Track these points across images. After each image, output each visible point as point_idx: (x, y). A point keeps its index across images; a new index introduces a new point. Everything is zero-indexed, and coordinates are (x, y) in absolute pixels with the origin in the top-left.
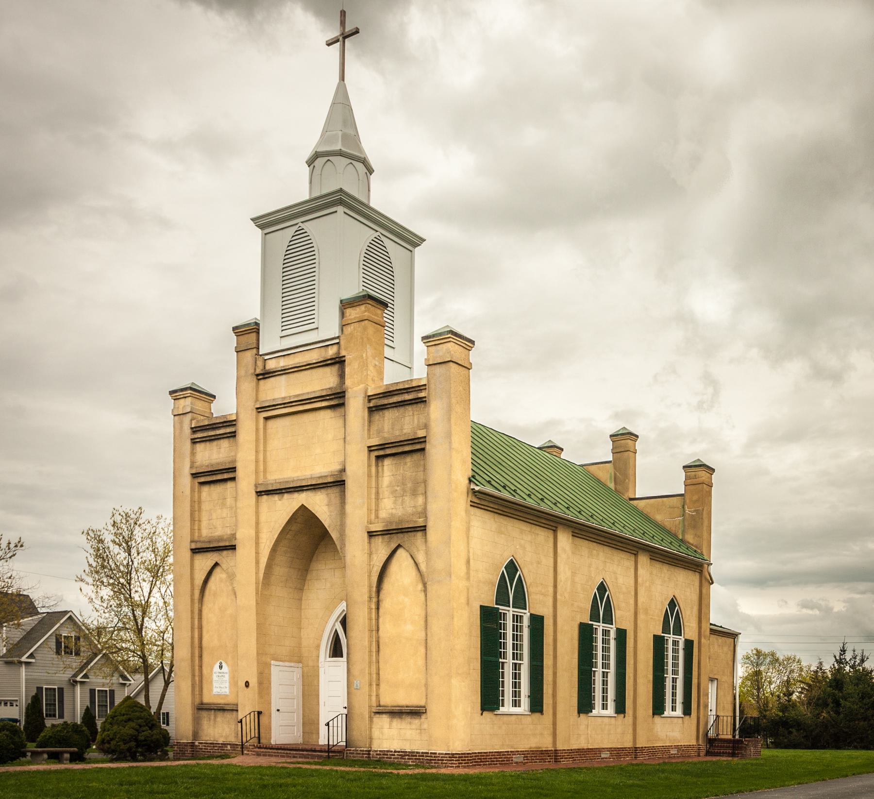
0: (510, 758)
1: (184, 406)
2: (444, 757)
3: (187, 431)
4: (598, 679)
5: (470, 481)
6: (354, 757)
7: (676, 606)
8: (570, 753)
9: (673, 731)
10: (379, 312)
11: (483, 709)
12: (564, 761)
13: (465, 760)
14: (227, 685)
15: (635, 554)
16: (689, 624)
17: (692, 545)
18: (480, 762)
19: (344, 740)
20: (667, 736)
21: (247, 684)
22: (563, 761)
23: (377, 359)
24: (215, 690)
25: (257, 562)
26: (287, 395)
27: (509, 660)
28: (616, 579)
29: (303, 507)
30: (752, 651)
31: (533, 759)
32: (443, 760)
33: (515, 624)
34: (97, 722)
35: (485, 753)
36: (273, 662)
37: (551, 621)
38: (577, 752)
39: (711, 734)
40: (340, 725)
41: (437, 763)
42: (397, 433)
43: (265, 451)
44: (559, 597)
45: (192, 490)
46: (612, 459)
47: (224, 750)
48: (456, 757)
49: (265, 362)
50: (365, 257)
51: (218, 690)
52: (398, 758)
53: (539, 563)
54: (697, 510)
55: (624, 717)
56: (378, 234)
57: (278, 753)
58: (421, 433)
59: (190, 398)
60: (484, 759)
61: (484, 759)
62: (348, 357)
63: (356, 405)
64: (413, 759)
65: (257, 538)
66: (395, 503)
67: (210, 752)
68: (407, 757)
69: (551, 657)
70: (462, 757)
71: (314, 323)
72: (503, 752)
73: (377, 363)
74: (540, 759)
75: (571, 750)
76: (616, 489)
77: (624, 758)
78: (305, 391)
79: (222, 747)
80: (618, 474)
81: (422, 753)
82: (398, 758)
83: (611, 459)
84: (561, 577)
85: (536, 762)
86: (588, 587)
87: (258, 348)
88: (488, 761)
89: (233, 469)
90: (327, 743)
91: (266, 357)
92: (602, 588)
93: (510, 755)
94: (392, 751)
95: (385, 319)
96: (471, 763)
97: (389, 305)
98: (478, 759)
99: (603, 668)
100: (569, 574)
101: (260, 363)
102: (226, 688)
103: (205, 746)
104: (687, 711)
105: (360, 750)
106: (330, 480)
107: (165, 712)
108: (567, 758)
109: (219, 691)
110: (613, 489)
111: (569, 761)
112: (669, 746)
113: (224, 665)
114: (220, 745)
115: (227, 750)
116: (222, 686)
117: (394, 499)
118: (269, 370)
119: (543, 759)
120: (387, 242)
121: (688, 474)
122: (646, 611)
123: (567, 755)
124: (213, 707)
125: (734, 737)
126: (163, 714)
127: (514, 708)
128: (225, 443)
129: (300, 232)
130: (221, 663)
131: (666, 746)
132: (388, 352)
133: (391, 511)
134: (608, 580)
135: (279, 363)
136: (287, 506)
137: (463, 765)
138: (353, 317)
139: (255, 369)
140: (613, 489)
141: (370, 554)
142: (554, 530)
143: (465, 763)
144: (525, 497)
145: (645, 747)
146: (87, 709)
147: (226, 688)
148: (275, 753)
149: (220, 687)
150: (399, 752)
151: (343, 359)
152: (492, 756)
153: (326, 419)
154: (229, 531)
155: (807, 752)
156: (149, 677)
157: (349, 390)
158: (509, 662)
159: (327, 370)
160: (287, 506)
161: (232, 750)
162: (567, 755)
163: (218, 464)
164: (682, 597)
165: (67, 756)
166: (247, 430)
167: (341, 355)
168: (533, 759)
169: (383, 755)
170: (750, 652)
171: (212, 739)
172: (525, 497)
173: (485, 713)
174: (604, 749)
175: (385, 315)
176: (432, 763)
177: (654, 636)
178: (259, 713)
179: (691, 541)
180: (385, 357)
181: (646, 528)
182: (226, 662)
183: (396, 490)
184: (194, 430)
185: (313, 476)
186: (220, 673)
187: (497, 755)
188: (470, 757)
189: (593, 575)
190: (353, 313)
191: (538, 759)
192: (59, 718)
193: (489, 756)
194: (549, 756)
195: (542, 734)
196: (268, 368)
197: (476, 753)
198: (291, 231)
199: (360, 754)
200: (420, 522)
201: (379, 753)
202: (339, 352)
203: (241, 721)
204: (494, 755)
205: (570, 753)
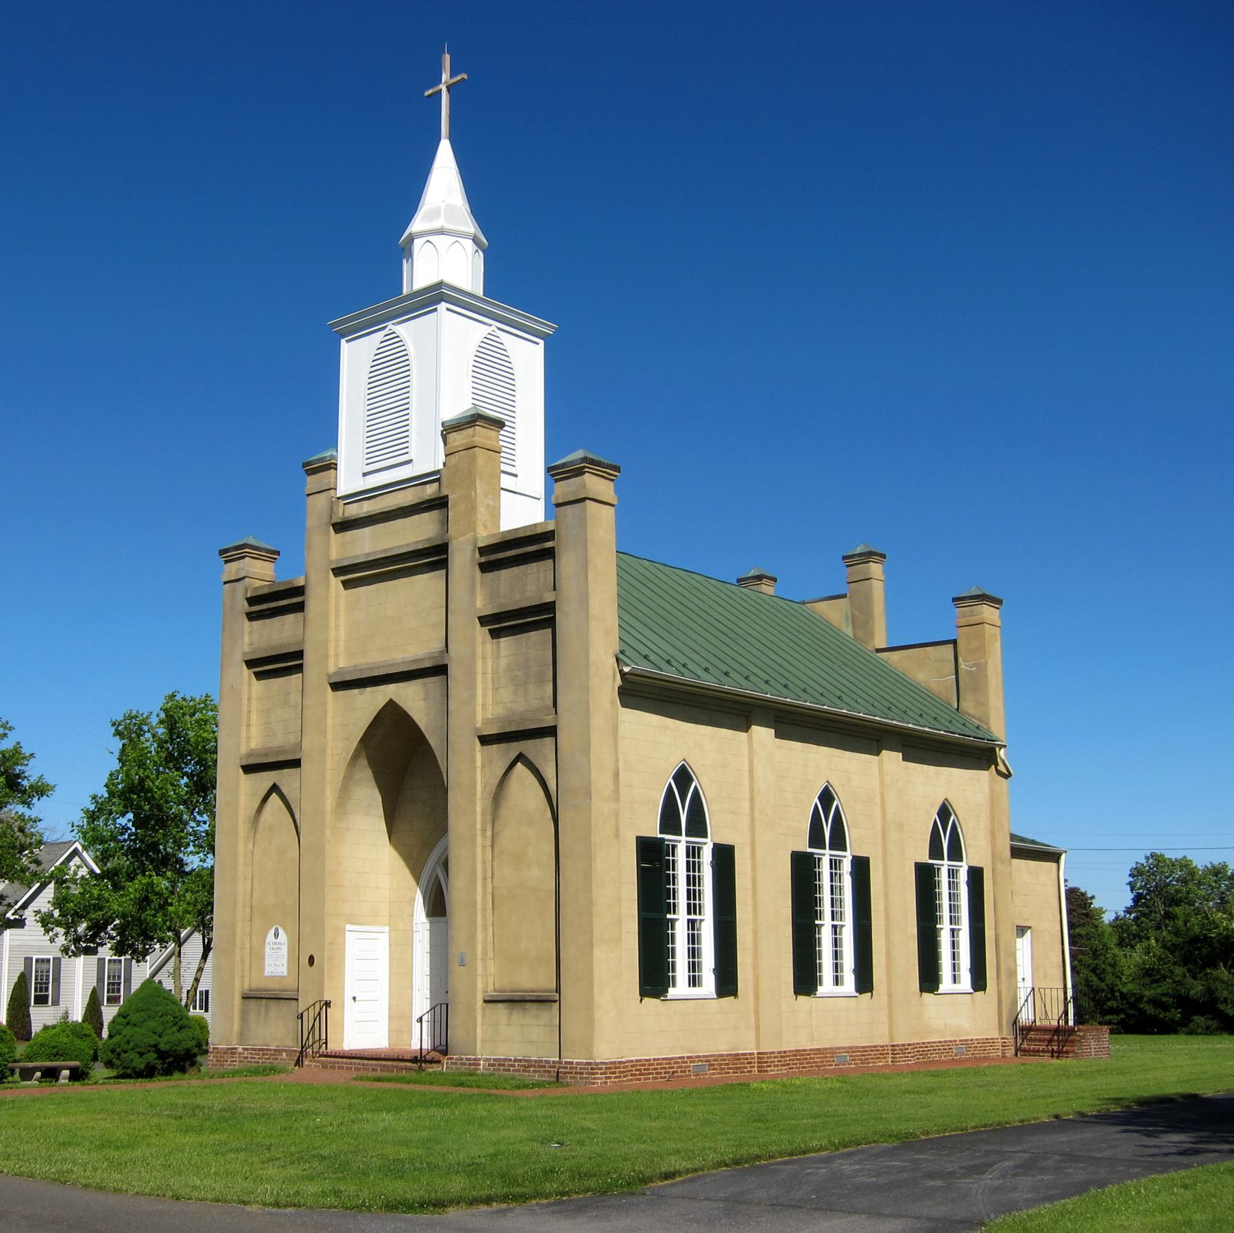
0: (686, 1067)
1: (238, 569)
4: (826, 936)
5: (618, 660)
7: (950, 815)
8: (782, 1057)
10: (493, 433)
11: (644, 993)
13: (615, 1073)
14: (285, 961)
15: (877, 741)
17: (974, 717)
18: (640, 1075)
20: (946, 1024)
22: (771, 1071)
23: (490, 496)
26: (371, 550)
29: (391, 704)
30: (1147, 858)
32: (582, 1073)
33: (691, 859)
34: (103, 1008)
35: (646, 1060)
37: (747, 851)
38: (794, 1055)
39: (1026, 1017)
41: (574, 1078)
42: (517, 597)
48: (602, 1069)
52: (519, 1071)
54: (979, 664)
55: (872, 995)
56: (493, 328)
57: (351, 1063)
58: (548, 598)
60: (645, 1070)
61: (645, 1070)
63: (462, 559)
66: (515, 693)
68: (532, 1069)
69: (750, 908)
70: (610, 1068)
71: (407, 453)
72: (675, 1058)
73: (491, 502)
74: (735, 1068)
75: (785, 1052)
76: (854, 635)
77: (874, 1063)
78: (397, 544)
80: (857, 613)
82: (519, 1071)
85: (729, 1073)
88: (652, 1074)
89: (299, 654)
90: (419, 1047)
92: (826, 797)
93: (687, 1062)
95: (501, 443)
96: (624, 1077)
97: (507, 423)
98: (636, 1070)
103: (251, 1054)
104: (979, 981)
105: (466, 1059)
106: (428, 664)
107: (204, 989)
108: (777, 1066)
109: (273, 970)
110: (851, 636)
111: (781, 1070)
112: (951, 1041)
113: (281, 931)
114: (272, 1052)
115: (281, 1059)
117: (514, 688)
118: (349, 517)
119: (739, 1068)
122: (900, 826)
123: (778, 1061)
124: (264, 994)
125: (1067, 1021)
126: (201, 992)
127: (692, 988)
128: (290, 619)
129: (394, 336)
130: (277, 930)
131: (945, 1042)
132: (506, 481)
135: (362, 507)
136: (372, 700)
137: (613, 1080)
138: (458, 444)
139: (331, 518)
140: (851, 636)
142: (747, 717)
143: (615, 1078)
144: (700, 672)
145: (909, 1045)
146: (94, 991)
148: (347, 1064)
150: (520, 1061)
152: (658, 1064)
153: (426, 585)
154: (292, 739)
156: (182, 935)
157: (454, 541)
158: (681, 917)
159: (425, 516)
160: (372, 700)
161: (289, 1060)
162: (778, 1061)
165: (66, 1073)
170: (1143, 861)
172: (700, 672)
173: (646, 1000)
174: (839, 1048)
175: (501, 437)
177: (916, 864)
179: (971, 711)
180: (502, 489)
181: (896, 696)
182: (284, 929)
183: (517, 676)
185: (405, 660)
186: (275, 944)
187: (666, 1064)
188: (624, 1067)
190: (458, 439)
191: (731, 1068)
192: (52, 1005)
193: (653, 1064)
194: (748, 1063)
197: (632, 1061)
198: (379, 336)
199: (465, 1064)
200: (548, 721)
203: (301, 1016)
204: (661, 1064)
205: (782, 1057)
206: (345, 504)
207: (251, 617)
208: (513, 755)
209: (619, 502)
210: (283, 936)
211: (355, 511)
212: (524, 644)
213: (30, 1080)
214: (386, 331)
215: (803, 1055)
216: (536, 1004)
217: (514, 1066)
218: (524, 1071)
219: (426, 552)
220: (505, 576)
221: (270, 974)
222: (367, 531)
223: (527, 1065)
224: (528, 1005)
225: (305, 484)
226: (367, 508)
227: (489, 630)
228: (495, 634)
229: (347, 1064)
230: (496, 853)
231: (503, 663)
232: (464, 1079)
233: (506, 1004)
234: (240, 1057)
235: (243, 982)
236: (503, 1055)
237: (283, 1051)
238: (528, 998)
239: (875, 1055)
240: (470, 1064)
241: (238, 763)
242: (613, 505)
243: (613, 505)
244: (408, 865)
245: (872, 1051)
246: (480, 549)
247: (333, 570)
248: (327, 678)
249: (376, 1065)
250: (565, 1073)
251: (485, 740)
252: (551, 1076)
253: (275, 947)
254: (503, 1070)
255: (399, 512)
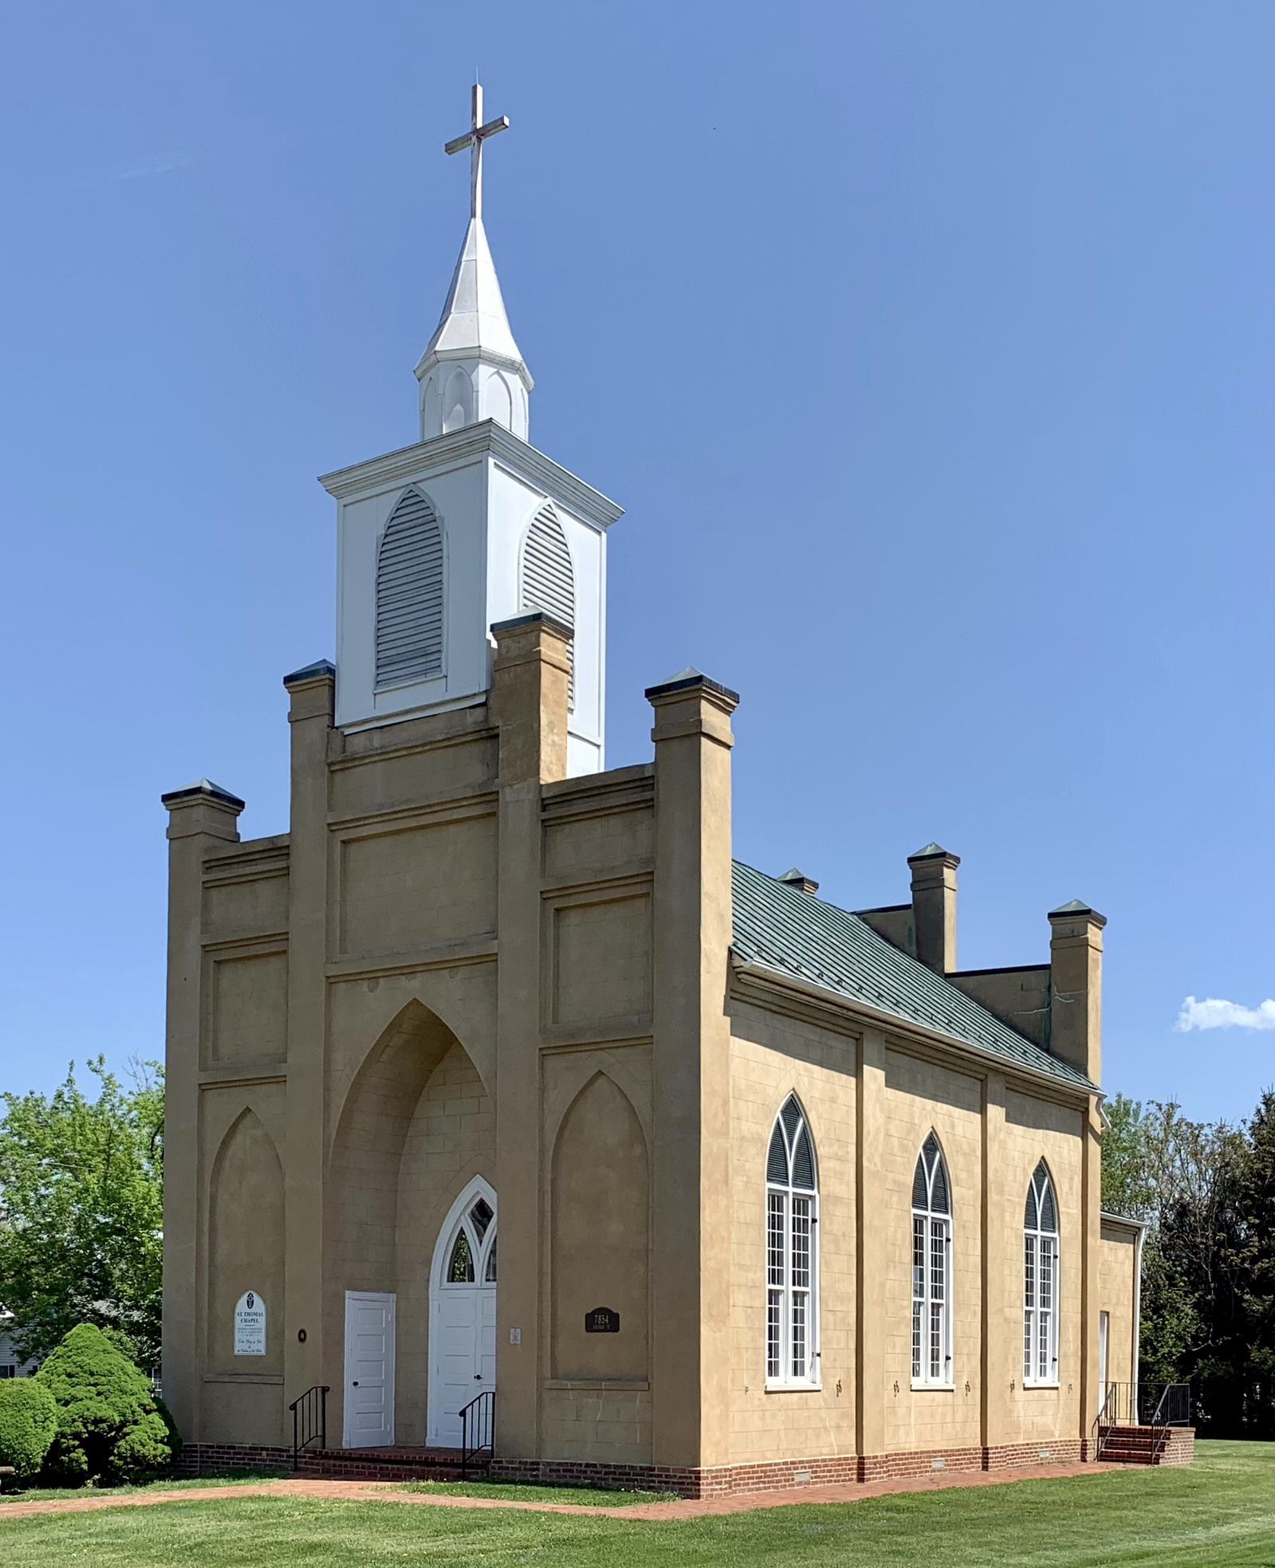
0: (789, 1475)
3: (196, 867)
9: (1042, 1414)
12: (876, 1478)
14: (262, 1337)
16: (1067, 1210)
19: (489, 1442)
20: (1033, 1423)
21: (302, 1336)
24: (239, 1348)
25: (327, 1106)
27: (927, 1299)
28: (953, 1127)
31: (840, 1475)
36: (348, 1293)
40: (483, 1411)
43: (343, 901)
44: (865, 1164)
45: (204, 974)
46: (911, 902)
47: (254, 1460)
49: (345, 741)
50: (529, 538)
51: (245, 1346)
53: (833, 1100)
59: (201, 807)
65: (328, 1061)
67: (228, 1463)
73: (556, 739)
81: (641, 1468)
83: (910, 902)
84: (869, 1125)
86: (910, 1144)
87: (333, 716)
91: (348, 731)
99: (794, 1284)
100: (881, 1120)
101: (337, 743)
102: (259, 1342)
103: (218, 1452)
111: (883, 1478)
113: (256, 1298)
120: (564, 519)
121: (1056, 927)
128: (265, 890)
134: (940, 1131)
141: (543, 1091)
142: (857, 1039)
147: (259, 1342)
149: (248, 1341)
151: (496, 731)
155: (1255, 1445)
164: (1057, 1159)
166: (309, 864)
167: (491, 726)
168: (840, 1475)
178: (325, 1390)
184: (209, 866)
189: (916, 1121)
195: (838, 1427)
196: (350, 749)
202: (486, 720)
203: (294, 1407)
209: (736, 743)
210: (259, 1305)
215: (902, 1459)
217: (585, 1472)
221: (241, 1353)
232: (897, 1501)
234: (202, 1457)
237: (262, 1449)
239: (968, 1459)
242: (728, 747)
243: (728, 747)
245: (966, 1454)
253: (249, 1318)
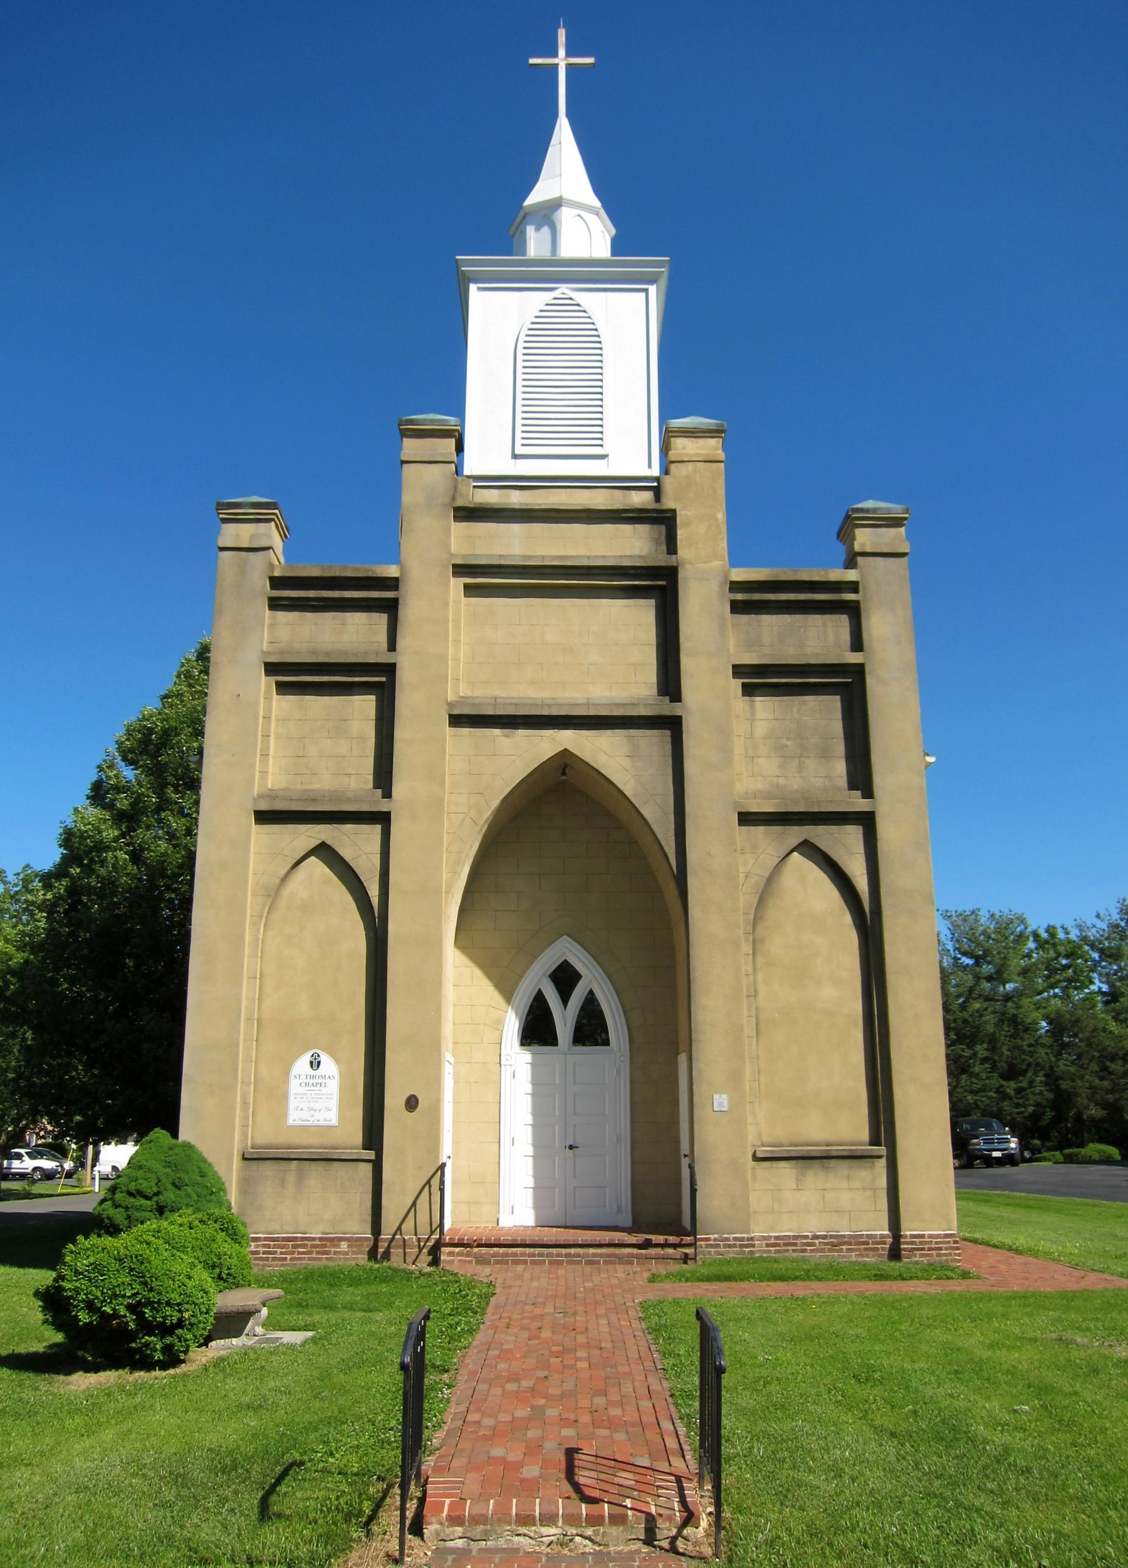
2: (944, 1243)
6: (718, 1253)
14: (334, 1103)
32: (940, 1249)
41: (928, 1255)
51: (305, 1115)
52: (822, 1251)
57: (540, 1255)
62: (684, 512)
64: (859, 1250)
68: (844, 1247)
79: (325, 1246)
94: (807, 1237)
105: (735, 1239)
113: (325, 1059)
115: (339, 1253)
116: (316, 1106)
117: (781, 759)
133: (775, 780)
150: (824, 1237)
157: (688, 566)
163: (328, 653)
169: (785, 1245)
171: (288, 1228)
176: (915, 1256)
182: (333, 1055)
183: (786, 746)
186: (314, 1077)
198: (547, 297)
199: (734, 1246)
201: (773, 1241)
206: (475, 487)
207: (275, 604)
208: (795, 841)
210: (328, 1065)
211: (491, 497)
212: (795, 709)
213: (237, 1335)
214: (556, 294)
216: (848, 1161)
218: (830, 1251)
219: (632, 572)
220: (770, 622)
222: (516, 528)
223: (836, 1242)
224: (833, 1162)
225: (400, 448)
226: (516, 499)
227: (744, 685)
228: (749, 690)
229: (530, 1255)
230: (758, 965)
231: (761, 729)
233: (793, 1162)
235: (244, 1134)
236: (790, 1231)
238: (834, 1154)
240: (741, 1246)
241: (250, 808)
244: (489, 976)
246: (732, 583)
247: (455, 566)
248: (445, 706)
249: (594, 1255)
250: (912, 1250)
251: (746, 819)
252: (880, 1256)
254: (794, 1251)
255: (582, 515)
